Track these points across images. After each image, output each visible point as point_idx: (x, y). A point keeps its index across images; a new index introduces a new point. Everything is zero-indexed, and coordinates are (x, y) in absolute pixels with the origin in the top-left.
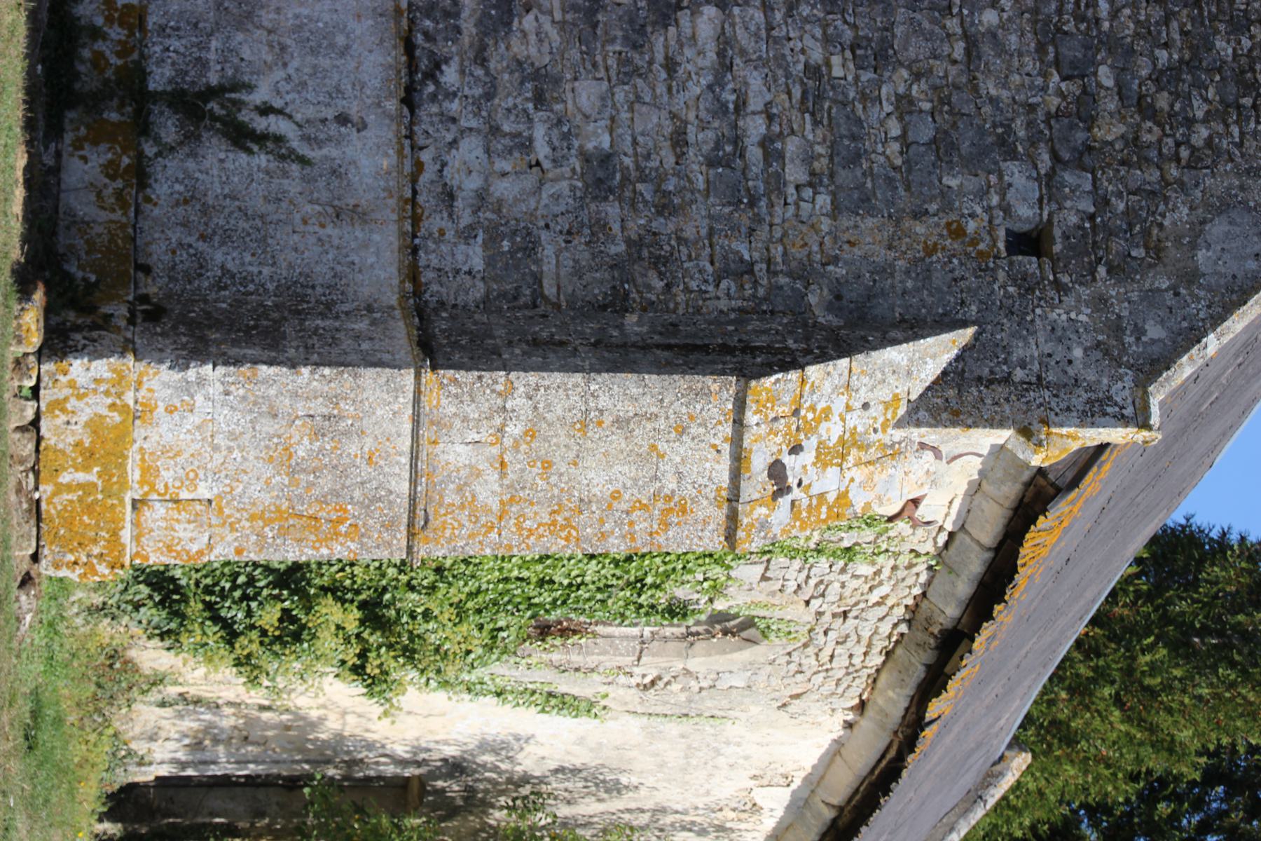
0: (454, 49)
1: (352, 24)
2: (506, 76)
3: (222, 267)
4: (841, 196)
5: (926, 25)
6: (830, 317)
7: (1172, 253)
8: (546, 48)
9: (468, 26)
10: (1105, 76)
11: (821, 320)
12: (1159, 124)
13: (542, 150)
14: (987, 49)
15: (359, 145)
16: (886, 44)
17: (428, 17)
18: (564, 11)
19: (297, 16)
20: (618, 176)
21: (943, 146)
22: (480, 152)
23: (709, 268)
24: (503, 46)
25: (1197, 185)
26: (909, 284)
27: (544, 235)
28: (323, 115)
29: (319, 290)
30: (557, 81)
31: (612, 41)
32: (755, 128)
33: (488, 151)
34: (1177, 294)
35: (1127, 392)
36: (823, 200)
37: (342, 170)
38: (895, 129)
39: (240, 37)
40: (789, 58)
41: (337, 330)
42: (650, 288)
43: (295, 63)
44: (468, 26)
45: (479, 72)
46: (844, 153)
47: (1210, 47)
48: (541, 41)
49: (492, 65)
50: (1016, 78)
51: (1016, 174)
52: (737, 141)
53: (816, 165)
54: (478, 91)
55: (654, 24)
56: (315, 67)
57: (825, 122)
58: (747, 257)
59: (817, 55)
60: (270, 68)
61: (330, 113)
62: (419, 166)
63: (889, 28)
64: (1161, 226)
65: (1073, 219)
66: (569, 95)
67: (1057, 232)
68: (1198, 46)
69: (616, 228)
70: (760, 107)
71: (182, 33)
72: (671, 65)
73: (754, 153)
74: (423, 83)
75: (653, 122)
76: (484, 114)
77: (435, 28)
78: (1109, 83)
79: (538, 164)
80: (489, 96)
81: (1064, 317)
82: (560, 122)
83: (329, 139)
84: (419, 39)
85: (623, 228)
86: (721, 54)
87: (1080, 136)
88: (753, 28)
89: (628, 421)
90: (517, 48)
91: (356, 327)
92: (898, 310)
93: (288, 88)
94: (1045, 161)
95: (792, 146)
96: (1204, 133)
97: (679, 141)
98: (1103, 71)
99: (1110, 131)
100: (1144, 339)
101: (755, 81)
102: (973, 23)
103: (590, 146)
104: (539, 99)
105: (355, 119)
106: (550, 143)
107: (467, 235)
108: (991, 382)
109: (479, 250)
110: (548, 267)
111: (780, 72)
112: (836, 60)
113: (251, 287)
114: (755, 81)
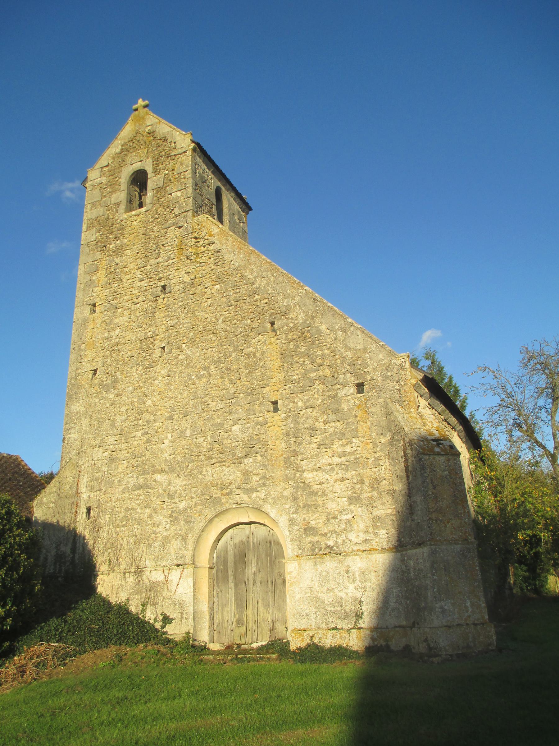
0: (323, 542)
1: (319, 570)
2: (329, 527)
3: (395, 603)
4: (353, 436)
5: (303, 419)
6: (388, 436)
7: (359, 354)
8: (320, 517)
9: (316, 539)
10: (313, 375)
11: (389, 438)
12: (325, 361)
13: (349, 516)
14: (308, 404)
15: (354, 567)
16: (309, 429)
17: (314, 550)
18: (309, 513)
19: (319, 586)
20: (354, 495)
21: (336, 412)
22: (352, 533)
23: (378, 468)
24: (320, 529)
25: (340, 351)
26: (376, 416)
27: (374, 514)
28: (347, 577)
29: (399, 575)
30: (329, 514)
31: (316, 500)
32: (336, 460)
33: (351, 531)
34: (370, 352)
35: (398, 361)
36: (354, 440)
37: (362, 571)
38: (332, 424)
39: (326, 602)
40: (316, 453)
41: (415, 569)
42: (386, 484)
43: (332, 586)
44: (316, 539)
45: (329, 535)
46: (341, 436)
47: (303, 352)
48: (318, 519)
49: (326, 531)
50: (315, 396)
51: (341, 393)
52: (341, 464)
53: (345, 443)
54: (334, 535)
55: (310, 489)
56: (333, 580)
57: (332, 442)
58: (373, 459)
59: (314, 445)
60: (334, 593)
61: (346, 575)
62: (358, 550)
63: (304, 428)
64: (352, 358)
65: (353, 378)
66: (333, 510)
67: (357, 382)
68: (303, 355)
69: (370, 494)
70: (330, 459)
71: (327, 618)
72: (321, 483)
73: (343, 459)
74: (334, 550)
75: (339, 487)
76: (341, 533)
77: (318, 548)
78: (315, 374)
79: (353, 517)
80: (336, 532)
81: (380, 378)
82: (341, 512)
83: (353, 575)
84: (321, 552)
85: (369, 492)
86: (316, 470)
87: (330, 379)
88: (309, 463)
89: (433, 486)
90: (320, 525)
91: (412, 564)
92: (383, 419)
93: (339, 587)
94: (337, 386)
95: (340, 450)
96: (326, 351)
97: (343, 479)
98: (312, 375)
99: (328, 372)
100: (383, 358)
101: (323, 461)
102: (302, 408)
103: (347, 503)
104: (335, 518)
105: (346, 568)
106: (347, 514)
107: (376, 535)
108: (400, 394)
109: (381, 531)
110: (383, 512)
111: (320, 455)
112: (315, 441)
113: (400, 594)
114: (323, 461)
